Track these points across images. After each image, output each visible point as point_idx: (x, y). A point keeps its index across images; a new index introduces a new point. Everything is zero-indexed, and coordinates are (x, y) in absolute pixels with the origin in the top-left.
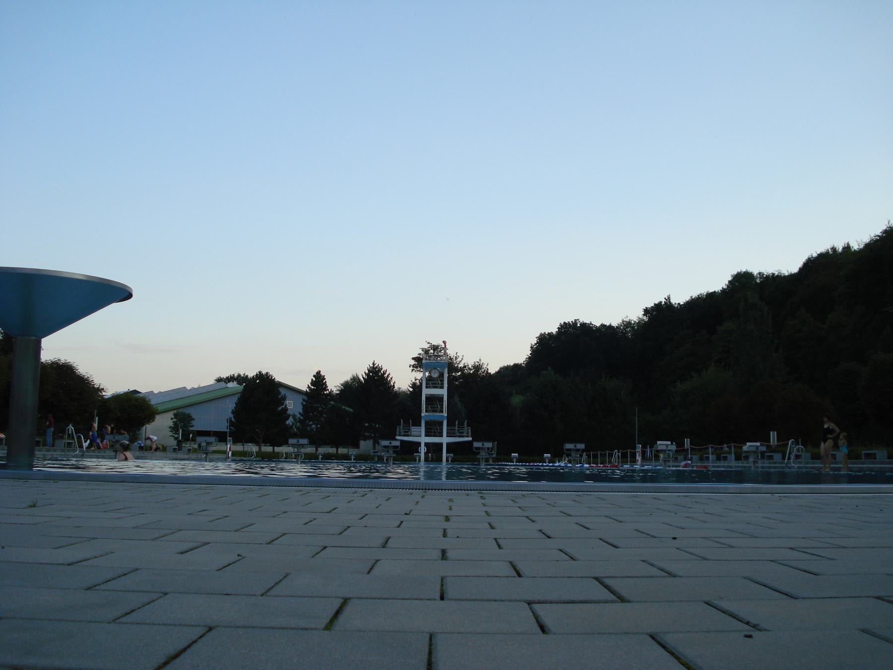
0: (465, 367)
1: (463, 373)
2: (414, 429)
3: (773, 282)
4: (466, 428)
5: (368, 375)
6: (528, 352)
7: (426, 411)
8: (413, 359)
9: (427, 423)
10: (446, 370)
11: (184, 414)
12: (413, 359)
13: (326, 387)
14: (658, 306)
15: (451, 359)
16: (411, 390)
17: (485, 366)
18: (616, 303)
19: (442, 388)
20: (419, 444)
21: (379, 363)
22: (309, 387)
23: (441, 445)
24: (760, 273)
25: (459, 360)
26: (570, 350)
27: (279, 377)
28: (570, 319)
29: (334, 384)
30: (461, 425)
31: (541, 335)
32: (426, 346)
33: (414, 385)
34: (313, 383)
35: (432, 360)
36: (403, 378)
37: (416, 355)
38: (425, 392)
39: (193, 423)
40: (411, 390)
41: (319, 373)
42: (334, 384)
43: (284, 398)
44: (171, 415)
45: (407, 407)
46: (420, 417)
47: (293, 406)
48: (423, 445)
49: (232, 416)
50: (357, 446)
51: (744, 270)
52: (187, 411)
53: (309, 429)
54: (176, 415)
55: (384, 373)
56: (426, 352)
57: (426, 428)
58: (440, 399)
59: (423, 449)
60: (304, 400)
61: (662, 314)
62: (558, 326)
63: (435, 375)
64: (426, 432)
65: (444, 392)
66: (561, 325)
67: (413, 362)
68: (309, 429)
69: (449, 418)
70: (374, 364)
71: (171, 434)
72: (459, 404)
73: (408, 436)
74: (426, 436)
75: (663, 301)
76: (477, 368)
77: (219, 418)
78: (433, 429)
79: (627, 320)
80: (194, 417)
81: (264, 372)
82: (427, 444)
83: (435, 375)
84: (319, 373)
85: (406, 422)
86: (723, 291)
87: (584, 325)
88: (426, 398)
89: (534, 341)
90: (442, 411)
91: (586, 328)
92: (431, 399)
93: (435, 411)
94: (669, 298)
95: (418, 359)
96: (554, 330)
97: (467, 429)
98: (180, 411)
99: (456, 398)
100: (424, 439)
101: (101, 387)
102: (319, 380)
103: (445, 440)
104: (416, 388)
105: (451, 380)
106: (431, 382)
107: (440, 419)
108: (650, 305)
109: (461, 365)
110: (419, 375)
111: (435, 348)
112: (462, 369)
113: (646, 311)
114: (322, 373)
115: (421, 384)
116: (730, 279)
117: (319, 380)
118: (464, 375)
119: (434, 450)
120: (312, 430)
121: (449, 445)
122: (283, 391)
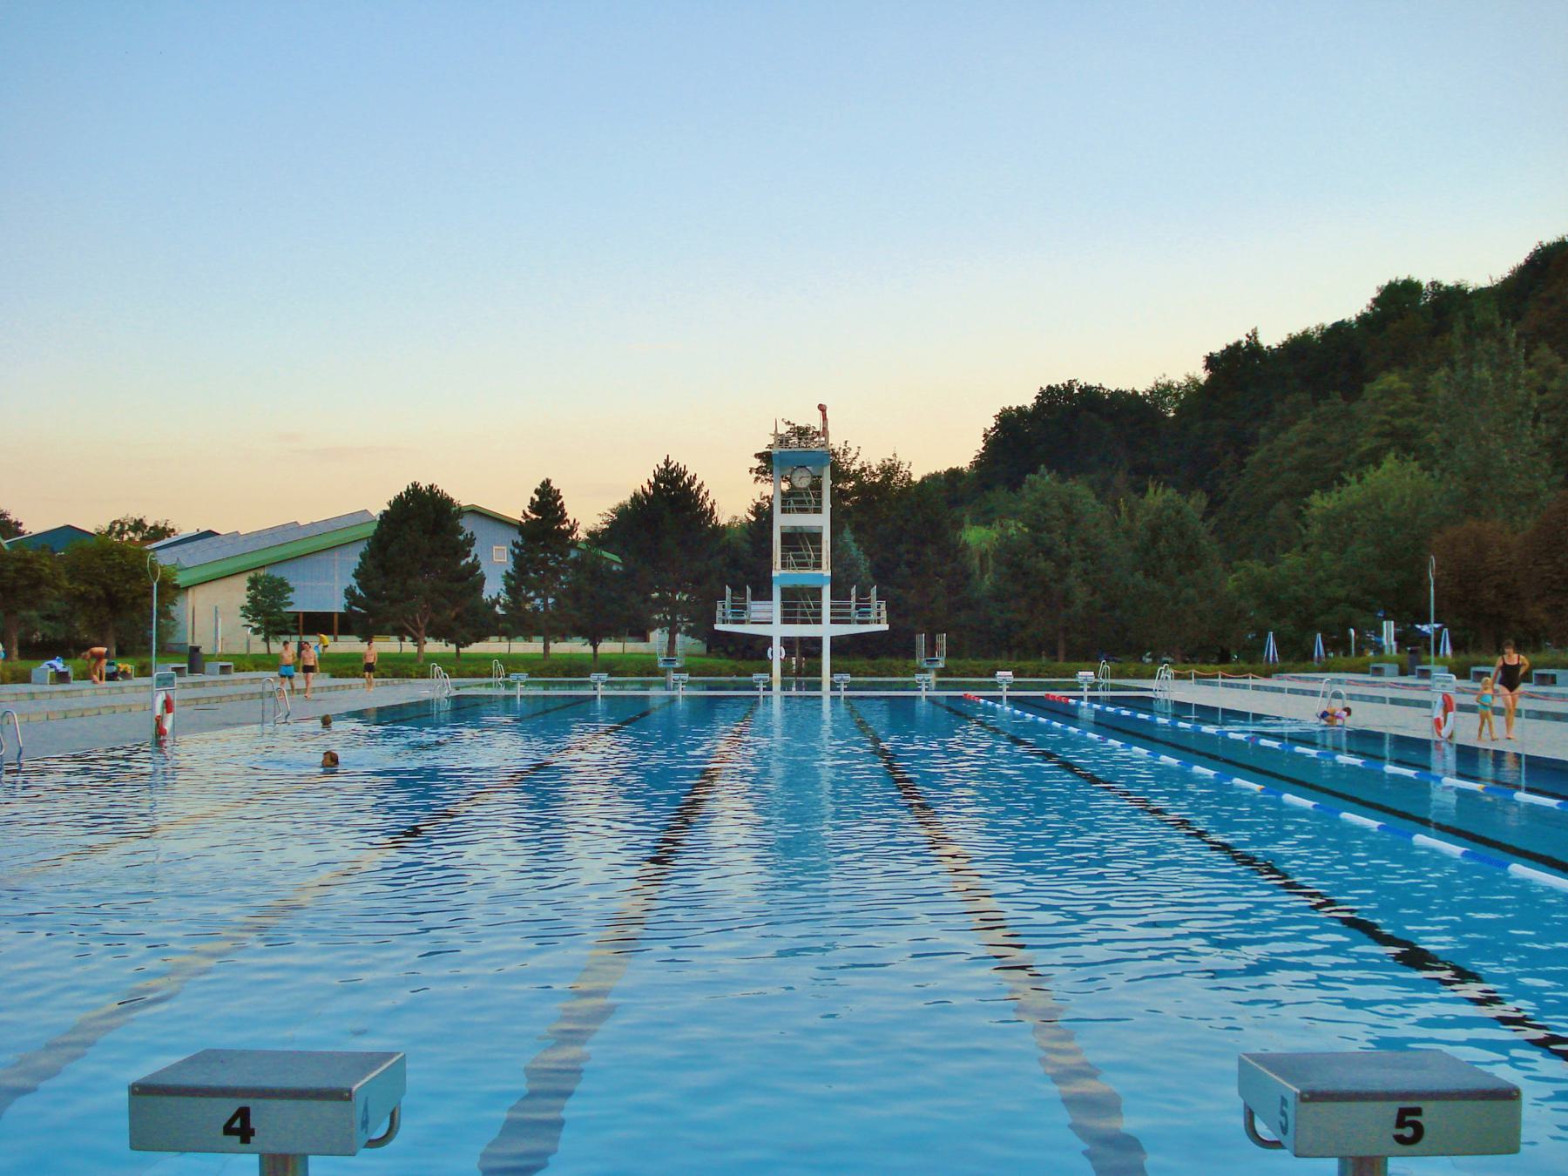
0: (863, 470)
1: (860, 483)
2: (756, 608)
3: (1451, 300)
4: (874, 603)
5: (655, 487)
6: (980, 445)
7: (784, 566)
8: (757, 456)
9: (784, 591)
10: (827, 472)
11: (271, 579)
12: (757, 456)
13: (564, 514)
14: (1233, 351)
15: (834, 454)
16: (753, 519)
17: (904, 468)
18: (1152, 348)
19: (818, 511)
20: (768, 641)
21: (679, 460)
22: (526, 516)
23: (817, 641)
24: (1433, 284)
25: (850, 456)
26: (1058, 433)
27: (462, 496)
28: (1059, 380)
29: (587, 513)
30: (863, 594)
31: (1004, 411)
32: (783, 429)
33: (758, 510)
34: (534, 507)
35: (795, 457)
36: (732, 495)
37: (763, 449)
38: (782, 521)
39: (291, 596)
40: (753, 519)
41: (546, 484)
42: (587, 513)
43: (471, 541)
44: (243, 582)
45: (743, 558)
46: (769, 581)
47: (495, 562)
48: (776, 642)
49: (354, 583)
50: (646, 639)
51: (1403, 277)
52: (277, 573)
53: (528, 607)
54: (254, 583)
55: (691, 483)
56: (782, 441)
57: (784, 605)
58: (815, 538)
59: (777, 653)
60: (515, 544)
61: (1238, 366)
62: (1037, 393)
63: (803, 481)
64: (784, 613)
65: (821, 522)
66: (1042, 392)
67: (757, 463)
68: (528, 607)
69: (835, 583)
70: (667, 463)
71: (246, 621)
72: (854, 546)
73: (742, 622)
74: (785, 621)
75: (1245, 339)
76: (889, 471)
77: (326, 589)
78: (799, 604)
79: (1164, 381)
80: (292, 584)
81: (424, 485)
82: (788, 643)
83: (803, 481)
84: (546, 484)
85: (738, 590)
86: (1363, 319)
87: (1087, 391)
88: (783, 535)
89: (991, 423)
90: (818, 565)
91: (1091, 399)
92: (793, 539)
93: (804, 565)
94: (1255, 333)
95: (765, 457)
96: (1028, 401)
97: (878, 607)
98: (262, 573)
99: (848, 535)
100: (778, 631)
101: (170, 526)
102: (547, 501)
103: (826, 631)
104: (763, 514)
105: (838, 496)
106: (795, 500)
107: (815, 584)
108: (1218, 347)
109: (856, 467)
110: (768, 489)
111: (802, 433)
112: (856, 476)
113: (1211, 362)
114: (554, 485)
115: (771, 506)
116: (1376, 295)
117: (547, 501)
118: (862, 488)
119: (807, 649)
120: (536, 609)
121: (841, 646)
122: (468, 525)
